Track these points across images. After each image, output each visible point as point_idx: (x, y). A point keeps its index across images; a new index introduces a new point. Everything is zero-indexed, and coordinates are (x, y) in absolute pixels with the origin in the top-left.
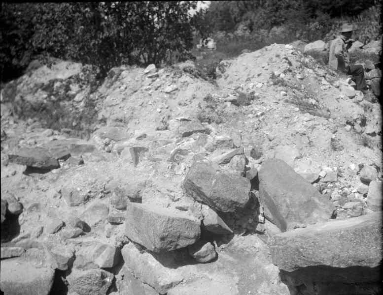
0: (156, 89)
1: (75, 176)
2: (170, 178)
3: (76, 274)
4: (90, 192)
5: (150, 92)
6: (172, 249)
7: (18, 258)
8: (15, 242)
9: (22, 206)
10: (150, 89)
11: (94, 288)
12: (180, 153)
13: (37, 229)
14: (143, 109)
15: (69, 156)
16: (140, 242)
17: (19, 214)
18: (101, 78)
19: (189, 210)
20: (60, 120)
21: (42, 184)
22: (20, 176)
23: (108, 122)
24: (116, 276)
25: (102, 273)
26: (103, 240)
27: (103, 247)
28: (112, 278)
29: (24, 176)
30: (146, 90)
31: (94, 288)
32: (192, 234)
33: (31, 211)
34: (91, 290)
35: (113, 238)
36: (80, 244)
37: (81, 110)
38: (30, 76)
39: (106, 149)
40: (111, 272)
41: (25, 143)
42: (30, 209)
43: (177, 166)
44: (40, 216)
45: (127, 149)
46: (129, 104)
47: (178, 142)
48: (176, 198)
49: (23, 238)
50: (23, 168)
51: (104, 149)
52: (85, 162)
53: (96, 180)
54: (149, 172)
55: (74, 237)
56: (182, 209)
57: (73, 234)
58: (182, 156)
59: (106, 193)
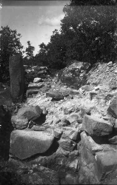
0: (111, 72)
1: (68, 103)
2: (104, 106)
3: (62, 140)
4: (72, 109)
5: (108, 73)
6: (98, 135)
7: (43, 131)
8: (43, 125)
9: (47, 112)
10: (108, 71)
11: (68, 147)
12: (110, 96)
13: (51, 121)
14: (105, 80)
15: (68, 95)
16: (87, 131)
17: (46, 115)
18: (90, 68)
19: (109, 120)
20: (74, 84)
21: (56, 105)
22: (50, 101)
23: (90, 84)
24: (77, 144)
25: (71, 142)
26: (74, 129)
27: (73, 132)
28: (76, 144)
29: (51, 101)
30: (107, 72)
31: (68, 147)
32: (108, 130)
33: (50, 114)
34: (67, 148)
35: (78, 128)
36: (65, 129)
37: (82, 80)
38: (68, 67)
39: (83, 94)
40: (75, 142)
41: (55, 90)
42: (50, 114)
43: (108, 102)
44: (53, 117)
45: (89, 93)
46: (99, 77)
47: (110, 91)
48: (104, 115)
49: (46, 124)
50: (51, 98)
51: (83, 94)
52: (74, 98)
53: (75, 105)
54: (95, 103)
55: (63, 126)
56: (106, 119)
57: (62, 125)
58: (110, 98)
59: (78, 110)
